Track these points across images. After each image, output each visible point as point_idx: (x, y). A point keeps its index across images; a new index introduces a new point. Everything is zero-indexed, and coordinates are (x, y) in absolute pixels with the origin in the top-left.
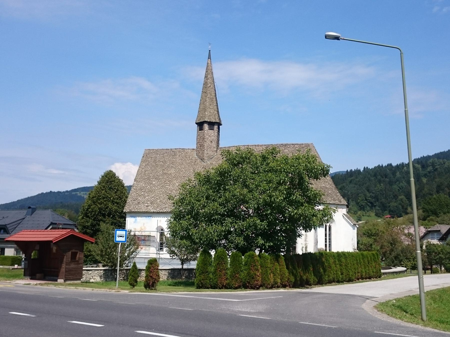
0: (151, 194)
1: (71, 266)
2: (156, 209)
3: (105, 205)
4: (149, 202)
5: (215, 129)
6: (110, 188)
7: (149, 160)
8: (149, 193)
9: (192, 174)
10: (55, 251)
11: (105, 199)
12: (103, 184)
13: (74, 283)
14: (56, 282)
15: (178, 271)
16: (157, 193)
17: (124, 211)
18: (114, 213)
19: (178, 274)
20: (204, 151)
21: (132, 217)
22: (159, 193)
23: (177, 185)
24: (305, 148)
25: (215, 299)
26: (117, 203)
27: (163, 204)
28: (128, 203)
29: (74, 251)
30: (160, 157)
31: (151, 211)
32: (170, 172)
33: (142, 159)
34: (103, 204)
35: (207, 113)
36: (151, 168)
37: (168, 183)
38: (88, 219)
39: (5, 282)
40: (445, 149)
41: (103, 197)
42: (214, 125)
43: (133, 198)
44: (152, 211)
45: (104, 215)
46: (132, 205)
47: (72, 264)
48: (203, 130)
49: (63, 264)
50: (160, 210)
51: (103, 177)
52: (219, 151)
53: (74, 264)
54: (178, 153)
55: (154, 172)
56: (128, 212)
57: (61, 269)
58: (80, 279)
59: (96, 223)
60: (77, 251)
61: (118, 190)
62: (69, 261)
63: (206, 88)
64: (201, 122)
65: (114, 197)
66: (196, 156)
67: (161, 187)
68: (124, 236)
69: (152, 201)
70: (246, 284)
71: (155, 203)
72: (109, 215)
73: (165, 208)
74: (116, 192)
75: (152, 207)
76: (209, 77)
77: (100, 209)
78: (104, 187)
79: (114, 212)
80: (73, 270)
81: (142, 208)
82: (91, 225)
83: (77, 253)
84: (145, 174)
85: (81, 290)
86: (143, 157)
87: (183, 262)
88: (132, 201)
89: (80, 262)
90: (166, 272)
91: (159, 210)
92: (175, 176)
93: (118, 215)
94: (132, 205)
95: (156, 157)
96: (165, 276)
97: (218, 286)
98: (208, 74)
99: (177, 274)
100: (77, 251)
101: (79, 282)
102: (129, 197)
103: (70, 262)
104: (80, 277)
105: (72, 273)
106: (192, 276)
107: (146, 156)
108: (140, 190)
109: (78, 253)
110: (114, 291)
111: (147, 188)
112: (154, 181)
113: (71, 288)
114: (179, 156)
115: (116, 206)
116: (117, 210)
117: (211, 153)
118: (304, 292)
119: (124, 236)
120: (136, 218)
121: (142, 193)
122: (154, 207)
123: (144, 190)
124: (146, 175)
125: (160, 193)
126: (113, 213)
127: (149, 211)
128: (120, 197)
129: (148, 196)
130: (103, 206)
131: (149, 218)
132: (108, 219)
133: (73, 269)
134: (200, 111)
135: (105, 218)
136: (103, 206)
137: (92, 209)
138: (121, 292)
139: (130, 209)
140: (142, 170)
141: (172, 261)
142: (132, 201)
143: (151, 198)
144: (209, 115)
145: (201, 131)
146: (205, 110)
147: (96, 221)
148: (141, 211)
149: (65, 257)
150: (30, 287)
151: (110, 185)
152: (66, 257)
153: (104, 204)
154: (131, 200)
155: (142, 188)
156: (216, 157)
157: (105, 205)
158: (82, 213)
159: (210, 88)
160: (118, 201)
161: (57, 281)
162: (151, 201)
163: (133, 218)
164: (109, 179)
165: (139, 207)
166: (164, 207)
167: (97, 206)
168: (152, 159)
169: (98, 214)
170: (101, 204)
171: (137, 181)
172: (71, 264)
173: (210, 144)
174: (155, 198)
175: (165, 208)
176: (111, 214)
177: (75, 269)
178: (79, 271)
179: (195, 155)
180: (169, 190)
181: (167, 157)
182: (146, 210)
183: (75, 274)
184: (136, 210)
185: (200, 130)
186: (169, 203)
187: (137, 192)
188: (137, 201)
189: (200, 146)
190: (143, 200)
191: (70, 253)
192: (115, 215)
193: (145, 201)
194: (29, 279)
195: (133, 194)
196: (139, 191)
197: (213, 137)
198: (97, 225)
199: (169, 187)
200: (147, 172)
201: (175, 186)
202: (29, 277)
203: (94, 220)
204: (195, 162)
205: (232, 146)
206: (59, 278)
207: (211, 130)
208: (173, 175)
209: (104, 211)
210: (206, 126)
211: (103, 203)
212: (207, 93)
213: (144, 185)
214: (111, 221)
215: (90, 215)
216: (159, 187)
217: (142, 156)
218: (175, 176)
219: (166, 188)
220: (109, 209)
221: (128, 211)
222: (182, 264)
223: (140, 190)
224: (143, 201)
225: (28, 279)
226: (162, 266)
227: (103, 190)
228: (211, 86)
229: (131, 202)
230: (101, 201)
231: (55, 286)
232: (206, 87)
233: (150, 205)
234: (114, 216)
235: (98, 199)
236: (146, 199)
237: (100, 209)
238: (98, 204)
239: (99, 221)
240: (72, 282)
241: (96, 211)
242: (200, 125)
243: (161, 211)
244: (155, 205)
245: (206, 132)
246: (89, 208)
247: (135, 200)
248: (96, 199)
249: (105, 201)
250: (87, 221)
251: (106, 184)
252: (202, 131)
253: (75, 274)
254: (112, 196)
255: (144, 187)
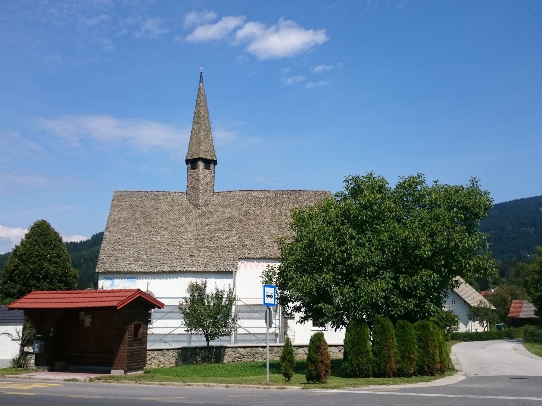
0: (132, 248)
1: (134, 347)
2: (143, 268)
3: (40, 266)
4: (131, 259)
5: (211, 169)
6: (45, 244)
7: (123, 205)
8: (130, 246)
9: (185, 224)
10: (88, 324)
11: (40, 258)
12: (36, 238)
13: (136, 374)
14: (109, 375)
15: (192, 350)
16: (141, 247)
17: (97, 270)
18: (52, 276)
19: (191, 354)
20: (198, 194)
21: (106, 278)
22: (143, 247)
23: (167, 237)
24: (322, 196)
25: (482, 397)
26: (56, 263)
27: (152, 261)
28: (101, 260)
29: (136, 322)
30: (138, 201)
31: (137, 270)
32: (155, 220)
33: (112, 204)
34: (36, 264)
35: (202, 148)
36: (127, 214)
37: (155, 234)
38: (13, 284)
39: (17, 377)
40: (539, 194)
41: (36, 254)
42: (210, 164)
43: (108, 253)
44: (138, 270)
45: (38, 279)
46: (107, 263)
47: (135, 345)
48: (197, 169)
49: (121, 345)
50: (149, 269)
51: (33, 228)
52: (215, 195)
53: (137, 343)
54: (161, 196)
55: (132, 220)
56: (103, 273)
57: (118, 353)
58: (141, 369)
59: (26, 289)
60: (140, 323)
61: (55, 246)
62: (132, 340)
63: (198, 117)
64: (194, 159)
65: (52, 255)
66: (187, 201)
67: (145, 239)
68: (272, 296)
69: (136, 257)
70: (424, 369)
71: (140, 260)
72: (45, 278)
73: (155, 267)
74: (53, 249)
75: (137, 266)
76: (202, 104)
77: (33, 271)
78: (36, 241)
79: (53, 274)
80: (135, 354)
81: (123, 267)
82: (18, 292)
83: (140, 325)
84: (120, 222)
85: (239, 389)
86: (113, 200)
87: (209, 337)
88: (107, 257)
89: (143, 341)
90: (174, 352)
91: (147, 269)
92: (164, 225)
93: (57, 279)
94: (107, 263)
95: (132, 201)
96: (174, 358)
97: (386, 373)
98: (200, 101)
99: (190, 355)
100: (140, 323)
101: (141, 372)
102: (101, 253)
103: (133, 341)
104: (143, 364)
105: (134, 358)
106: (211, 357)
107: (118, 199)
108: (116, 243)
109: (142, 326)
110: (275, 388)
111: (126, 240)
112: (134, 231)
113: (250, 387)
114: (164, 200)
115: (55, 267)
116: (56, 272)
117: (207, 198)
118: (520, 376)
119: (272, 296)
120: (112, 280)
121: (120, 247)
122: (140, 265)
123: (121, 243)
124: (122, 223)
125: (146, 247)
126: (51, 276)
127: (133, 270)
128: (58, 255)
129: (128, 251)
130: (36, 266)
131: (133, 279)
132: (43, 284)
133: (136, 353)
134: (192, 145)
135: (39, 283)
136: (36, 266)
137: (21, 271)
138: (286, 390)
139: (105, 267)
140: (114, 217)
141: (164, 337)
142: (107, 257)
143: (133, 254)
144: (204, 150)
145: (193, 170)
146: (199, 144)
147: (27, 286)
148: (122, 270)
149: (127, 333)
150: (78, 386)
151: (44, 239)
152: (129, 333)
153: (37, 263)
154: (105, 255)
155: (119, 241)
156: (213, 203)
157: (40, 266)
158: (5, 276)
159: (204, 118)
160: (57, 260)
161: (110, 373)
162: (134, 257)
163: (108, 280)
164: (43, 232)
165: (119, 266)
166: (154, 265)
167: (28, 266)
168: (127, 203)
169: (29, 277)
170: (34, 263)
171: (110, 231)
172: (133, 345)
173: (206, 186)
174: (140, 254)
175: (155, 267)
176: (47, 278)
177: (139, 352)
178: (142, 355)
179: (186, 199)
180: (157, 243)
181: (148, 202)
182: (129, 270)
183: (138, 360)
184: (115, 270)
185: (192, 169)
186: (160, 260)
187: (112, 246)
188: (113, 257)
189: (193, 189)
190: (123, 256)
191: (133, 326)
192: (54, 279)
193: (126, 257)
194: (47, 371)
195: (106, 249)
196: (114, 244)
197: (209, 179)
198: (26, 291)
199: (157, 239)
200: (122, 220)
201: (166, 238)
202: (46, 367)
203: (23, 285)
204: (187, 208)
205: (232, 190)
206: (114, 367)
207: (207, 170)
208: (160, 224)
209: (37, 273)
210: (201, 165)
211: (36, 262)
212: (201, 123)
213: (120, 237)
214: (48, 286)
215: (18, 278)
216: (142, 239)
217: (112, 199)
218: (164, 225)
219: (153, 241)
220: (46, 270)
221: (103, 270)
222: (208, 341)
223: (116, 243)
224: (122, 258)
225: (45, 371)
226: (151, 344)
227: (35, 245)
228: (206, 116)
229: (105, 259)
230: (34, 261)
231: (136, 382)
232: (199, 116)
233: (134, 262)
234: (51, 280)
235: (29, 257)
236: (126, 254)
237: (33, 271)
238: (29, 264)
239: (31, 286)
240: (134, 373)
241: (26, 273)
242: (192, 163)
243: (151, 270)
244: (140, 262)
245: (201, 171)
246: (16, 270)
247: (111, 256)
248: (27, 257)
249: (40, 260)
250: (12, 287)
251: (38, 238)
252: (195, 170)
253: (138, 360)
254: (49, 254)
255: (120, 239)
